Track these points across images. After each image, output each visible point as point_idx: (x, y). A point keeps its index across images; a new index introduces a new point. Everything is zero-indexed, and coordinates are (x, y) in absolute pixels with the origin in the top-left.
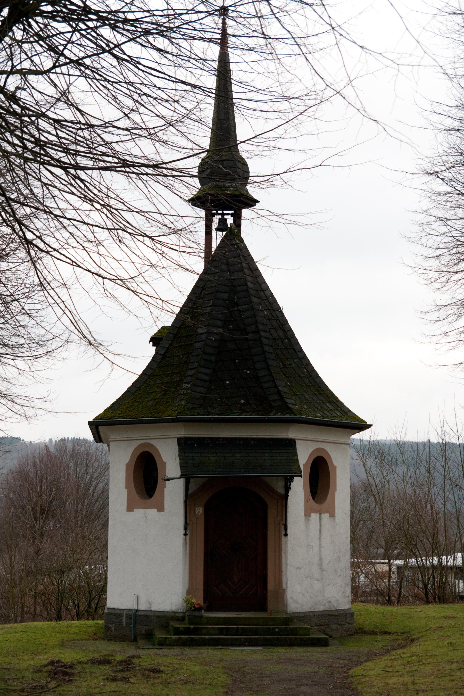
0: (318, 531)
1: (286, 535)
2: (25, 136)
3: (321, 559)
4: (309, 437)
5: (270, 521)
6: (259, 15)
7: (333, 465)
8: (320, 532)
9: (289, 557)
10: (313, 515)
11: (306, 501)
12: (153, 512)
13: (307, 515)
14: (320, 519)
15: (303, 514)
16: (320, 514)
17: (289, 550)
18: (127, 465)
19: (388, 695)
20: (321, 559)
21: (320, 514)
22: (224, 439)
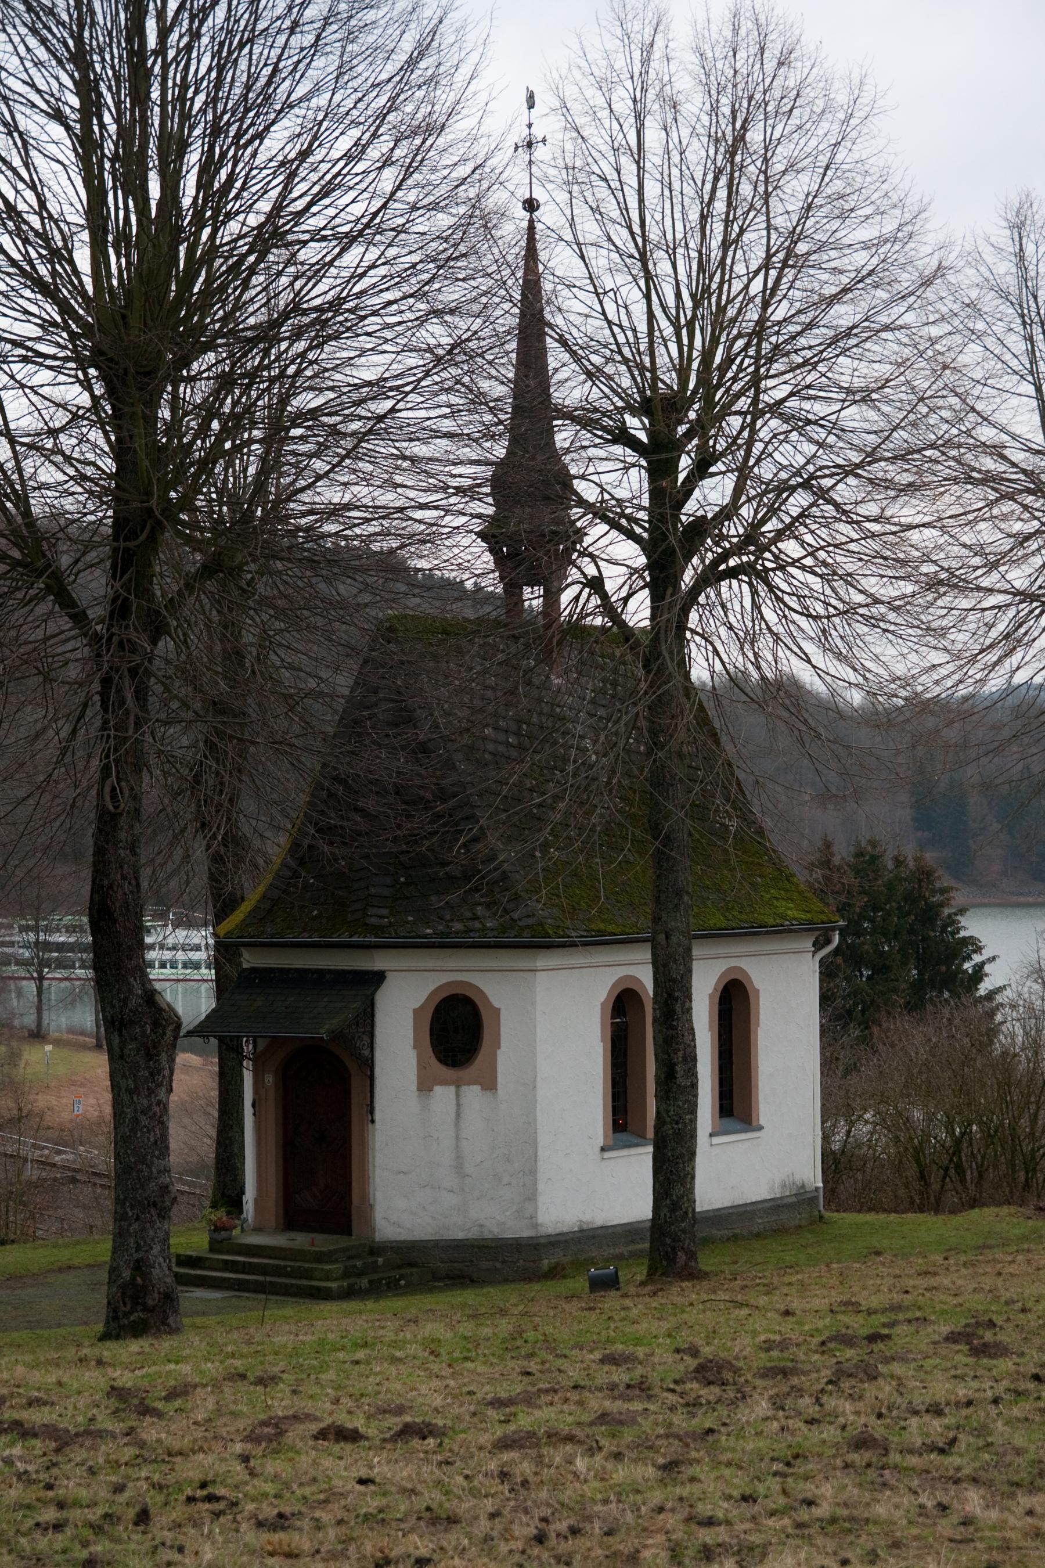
0: (453, 1115)
1: (373, 1121)
2: (773, 273)
3: (459, 1156)
4: (430, 964)
5: (355, 1100)
6: (575, 188)
7: (492, 1006)
8: (458, 1114)
9: (378, 1155)
10: (438, 1089)
11: (422, 1068)
12: (472, 1093)
13: (425, 1086)
14: (458, 1095)
15: (414, 1086)
16: (458, 1087)
17: (377, 1146)
18: (602, 1004)
19: (1036, 1378)
20: (459, 1156)
21: (458, 1087)
22: (296, 970)
